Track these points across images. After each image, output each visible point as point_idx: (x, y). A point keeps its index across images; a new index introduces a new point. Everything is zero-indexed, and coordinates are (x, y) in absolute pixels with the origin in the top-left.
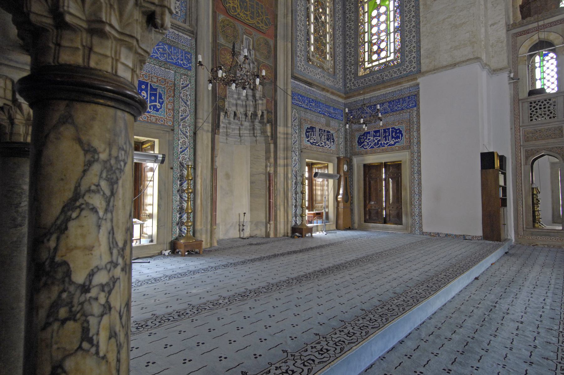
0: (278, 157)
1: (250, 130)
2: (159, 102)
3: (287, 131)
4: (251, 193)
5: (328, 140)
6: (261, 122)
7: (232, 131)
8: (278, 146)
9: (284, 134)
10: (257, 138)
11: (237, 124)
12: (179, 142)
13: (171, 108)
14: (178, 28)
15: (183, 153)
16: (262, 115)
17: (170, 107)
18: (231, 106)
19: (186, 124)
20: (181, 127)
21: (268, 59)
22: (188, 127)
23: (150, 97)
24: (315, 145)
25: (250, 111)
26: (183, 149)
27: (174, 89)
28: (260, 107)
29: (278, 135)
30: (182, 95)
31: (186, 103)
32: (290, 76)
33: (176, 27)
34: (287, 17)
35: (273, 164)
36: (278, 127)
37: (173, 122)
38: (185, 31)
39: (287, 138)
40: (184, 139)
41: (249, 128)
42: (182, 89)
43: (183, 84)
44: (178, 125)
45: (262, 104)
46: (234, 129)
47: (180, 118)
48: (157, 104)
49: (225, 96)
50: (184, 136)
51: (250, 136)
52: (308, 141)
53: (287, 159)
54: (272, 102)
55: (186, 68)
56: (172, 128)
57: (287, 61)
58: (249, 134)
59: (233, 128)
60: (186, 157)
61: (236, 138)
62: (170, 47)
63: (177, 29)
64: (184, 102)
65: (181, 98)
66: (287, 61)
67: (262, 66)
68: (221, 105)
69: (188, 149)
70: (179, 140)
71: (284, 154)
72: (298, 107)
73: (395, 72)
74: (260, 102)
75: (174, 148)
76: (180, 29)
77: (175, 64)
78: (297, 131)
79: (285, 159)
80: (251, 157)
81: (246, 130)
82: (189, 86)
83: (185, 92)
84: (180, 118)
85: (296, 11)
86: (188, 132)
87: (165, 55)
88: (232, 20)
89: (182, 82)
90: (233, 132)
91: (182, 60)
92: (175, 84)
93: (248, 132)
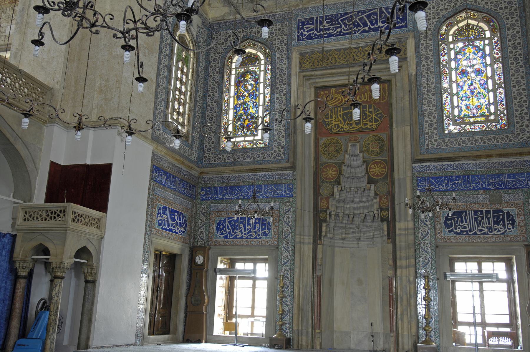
2: (268, 229)
5: (497, 223)
7: (364, 234)
13: (276, 231)
17: (275, 230)
20: (284, 244)
21: (379, 154)
23: (262, 226)
24: (467, 234)
29: (398, 232)
30: (285, 219)
31: (288, 225)
36: (397, 223)
37: (278, 242)
40: (286, 254)
42: (285, 214)
43: (286, 210)
48: (267, 230)
52: (452, 231)
54: (387, 198)
55: (289, 197)
56: (277, 246)
59: (364, 231)
60: (287, 268)
62: (276, 185)
64: (287, 224)
67: (371, 165)
69: (289, 261)
70: (282, 255)
73: (452, 143)
75: (278, 261)
77: (280, 196)
81: (377, 231)
82: (291, 210)
86: (290, 247)
87: (273, 193)
89: (285, 209)
90: (365, 235)
91: (285, 192)
92: (279, 212)
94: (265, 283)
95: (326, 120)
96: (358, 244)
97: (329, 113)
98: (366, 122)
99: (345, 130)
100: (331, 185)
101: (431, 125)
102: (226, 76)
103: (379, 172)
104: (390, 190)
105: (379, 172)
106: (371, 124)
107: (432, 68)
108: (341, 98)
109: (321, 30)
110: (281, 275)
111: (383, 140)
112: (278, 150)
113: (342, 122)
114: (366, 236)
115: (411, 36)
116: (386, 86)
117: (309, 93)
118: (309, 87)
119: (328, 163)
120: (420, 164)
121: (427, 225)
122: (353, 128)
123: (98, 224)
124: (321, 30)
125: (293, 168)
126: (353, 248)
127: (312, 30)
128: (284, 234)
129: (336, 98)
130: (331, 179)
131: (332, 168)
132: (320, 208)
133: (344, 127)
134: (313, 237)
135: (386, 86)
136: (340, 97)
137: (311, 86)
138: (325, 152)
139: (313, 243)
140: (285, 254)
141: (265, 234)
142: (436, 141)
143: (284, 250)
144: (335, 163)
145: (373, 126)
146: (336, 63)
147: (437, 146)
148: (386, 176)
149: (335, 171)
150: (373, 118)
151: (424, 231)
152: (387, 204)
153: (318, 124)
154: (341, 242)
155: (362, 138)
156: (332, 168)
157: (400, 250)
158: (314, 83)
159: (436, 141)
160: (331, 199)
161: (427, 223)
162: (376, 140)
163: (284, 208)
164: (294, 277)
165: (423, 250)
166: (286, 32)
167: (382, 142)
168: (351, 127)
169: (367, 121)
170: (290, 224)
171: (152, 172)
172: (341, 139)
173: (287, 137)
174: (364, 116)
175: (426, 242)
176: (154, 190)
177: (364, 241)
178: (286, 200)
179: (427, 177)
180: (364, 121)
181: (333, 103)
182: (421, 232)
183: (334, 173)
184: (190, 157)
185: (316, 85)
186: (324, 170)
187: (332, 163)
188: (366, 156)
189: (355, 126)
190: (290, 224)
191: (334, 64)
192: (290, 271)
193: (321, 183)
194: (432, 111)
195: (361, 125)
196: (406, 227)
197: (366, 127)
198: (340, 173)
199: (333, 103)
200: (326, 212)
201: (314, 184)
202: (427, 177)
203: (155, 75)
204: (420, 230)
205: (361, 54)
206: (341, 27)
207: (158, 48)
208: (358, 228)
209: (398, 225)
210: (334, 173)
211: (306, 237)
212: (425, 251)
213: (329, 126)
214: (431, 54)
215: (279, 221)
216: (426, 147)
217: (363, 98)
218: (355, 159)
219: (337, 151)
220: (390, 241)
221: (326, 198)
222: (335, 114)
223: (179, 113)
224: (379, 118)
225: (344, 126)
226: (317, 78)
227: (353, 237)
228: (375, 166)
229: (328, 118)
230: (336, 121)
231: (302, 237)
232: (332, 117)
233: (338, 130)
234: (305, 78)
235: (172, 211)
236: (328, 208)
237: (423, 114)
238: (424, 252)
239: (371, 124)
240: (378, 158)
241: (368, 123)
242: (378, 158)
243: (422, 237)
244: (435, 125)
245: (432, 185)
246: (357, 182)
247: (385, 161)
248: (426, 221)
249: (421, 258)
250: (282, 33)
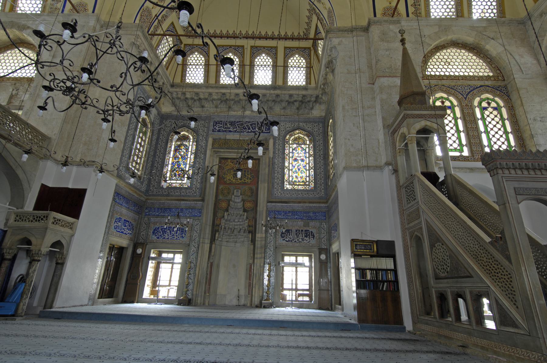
29: (257, 239)
46: (239, 238)
54: (253, 220)
62: (192, 209)
94: (179, 266)
102: (169, 146)
109: (225, 128)
123: (71, 226)
124: (225, 128)
125: (203, 200)
127: (221, 127)
141: (183, 237)
142: (280, 192)
151: (270, 239)
159: (280, 192)
160: (222, 219)
166: (206, 126)
171: (114, 196)
176: (114, 207)
178: (197, 218)
184: (141, 189)
190: (198, 232)
198: (229, 205)
200: (219, 226)
203: (124, 139)
206: (236, 128)
207: (128, 123)
208: (236, 236)
223: (137, 163)
235: (125, 220)
236: (220, 224)
250: (204, 126)
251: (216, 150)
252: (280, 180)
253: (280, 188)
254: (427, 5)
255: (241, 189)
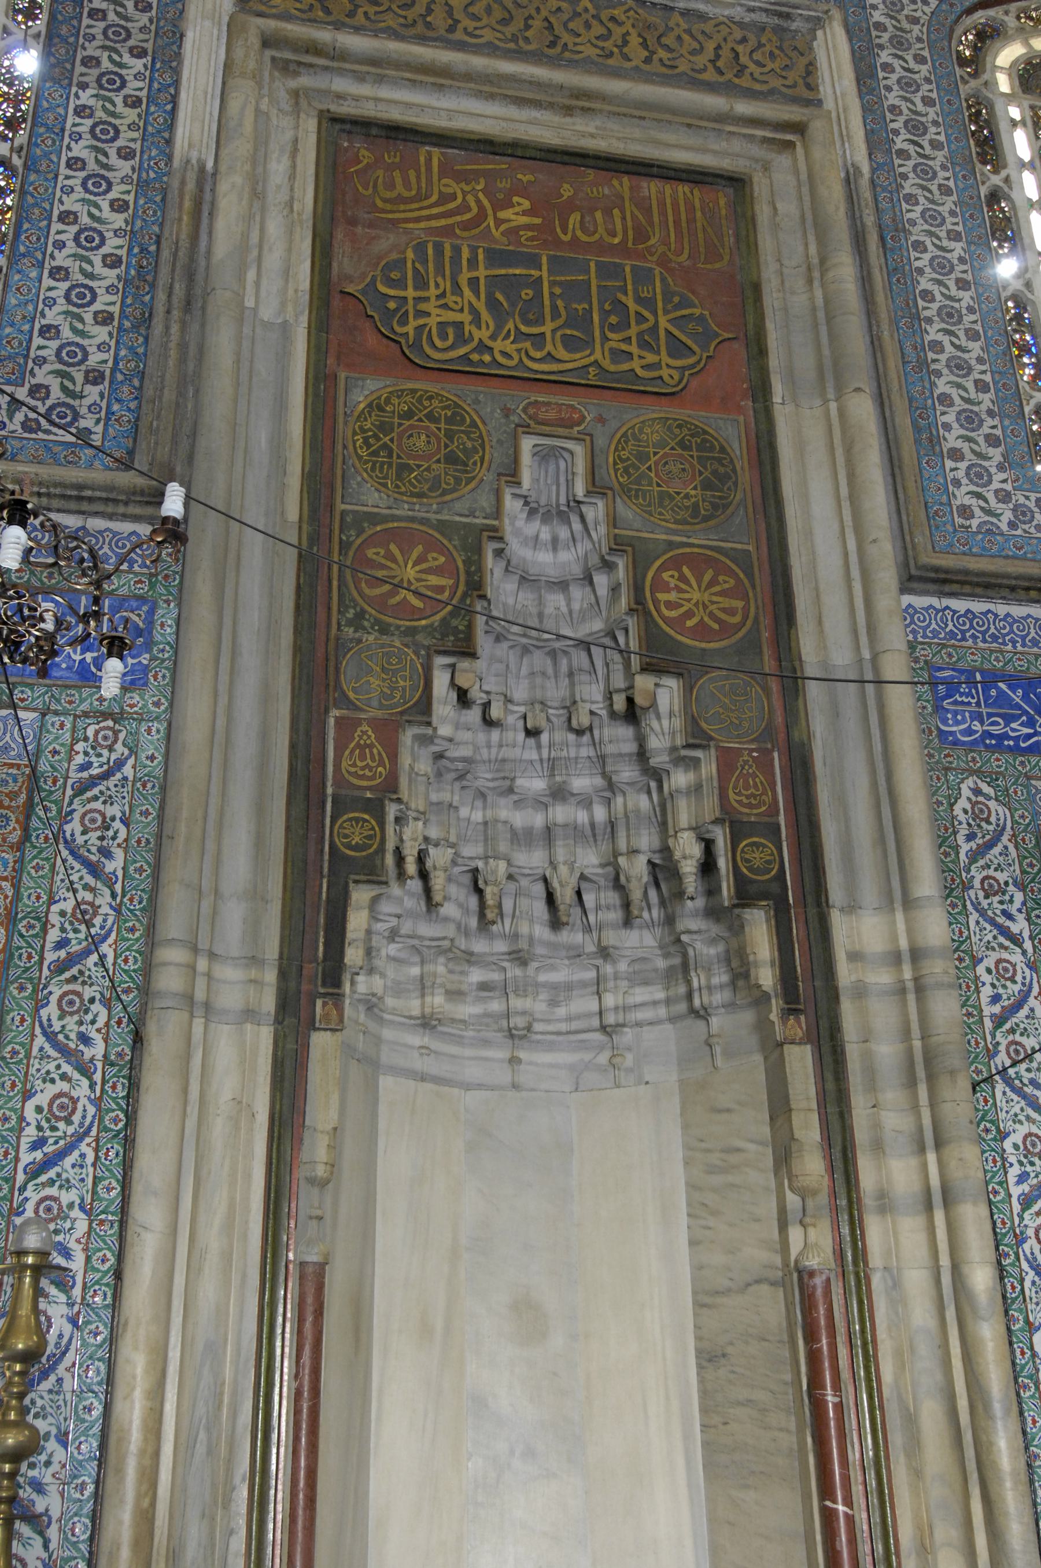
0: (861, 1135)
1: (669, 976)
3: (910, 931)
4: (705, 1444)
6: (714, 912)
7: (553, 1003)
8: (853, 1052)
9: (895, 958)
10: (714, 1021)
11: (576, 954)
12: (30, 1106)
14: (80, 498)
15: (52, 1173)
16: (708, 867)
18: (503, 847)
19: (88, 992)
20: (51, 1011)
21: (706, 519)
22: (96, 1007)
25: (634, 852)
26: (49, 1149)
27: (30, 805)
28: (684, 814)
29: (845, 974)
30: (74, 827)
31: (95, 870)
32: (887, 576)
33: (63, 497)
34: (824, 270)
35: (823, 1198)
38: (115, 501)
39: (920, 989)
40: (62, 1086)
41: (661, 964)
42: (79, 791)
43: (85, 767)
44: (28, 1005)
45: (697, 789)
46: (559, 993)
47: (50, 957)
49: (390, 786)
50: (67, 1068)
51: (672, 1019)
53: (939, 1144)
54: (766, 767)
57: (854, 499)
58: (668, 1002)
59: (554, 987)
61: (583, 1046)
63: (73, 505)
65: (977, 906)
66: (854, 499)
67: (662, 568)
68: (356, 840)
69: (86, 1148)
71: (915, 1108)
72: (998, 762)
74: (680, 779)
76: (90, 499)
78: (1020, 926)
79: (922, 1150)
80: (687, 1163)
81: (646, 983)
82: (128, 770)
83: (97, 805)
84: (50, 957)
85: (901, 229)
86: (98, 1039)
88: (432, 388)
89: (79, 759)
90: (561, 1011)
93: (661, 995)
95: (383, 289)
96: (514, 1061)
97: (404, 261)
98: (624, 347)
99: (500, 359)
100: (417, 647)
101: (970, 420)
103: (711, 615)
104: (779, 719)
105: (711, 615)
106: (651, 358)
107: (942, 174)
108: (478, 201)
110: (21, 1253)
111: (723, 449)
112: (64, 389)
113: (485, 316)
114: (569, 1019)
115: (836, 14)
116: (722, 202)
117: (289, 135)
118: (287, 108)
119: (394, 518)
120: (935, 601)
121: (1016, 940)
122: (550, 357)
126: (480, 1086)
128: (53, 935)
129: (445, 198)
130: (415, 614)
131: (419, 549)
132: (339, 781)
133: (498, 345)
134: (283, 975)
135: (722, 202)
136: (470, 199)
137: (303, 103)
138: (375, 453)
139: (278, 1021)
140: (52, 1090)
142: (1004, 497)
143: (43, 1057)
144: (442, 526)
145: (665, 373)
146: (451, 29)
147: (1012, 525)
148: (751, 645)
149: (438, 571)
150: (662, 334)
151: (1003, 972)
152: (767, 799)
153: (336, 302)
154: (416, 1039)
155: (601, 420)
156: (419, 549)
157: (872, 1085)
158: (326, 93)
159: (1004, 497)
161: (1015, 928)
162: (683, 445)
163: (71, 752)
164: (118, 1274)
165: (1014, 1089)
167: (719, 460)
168: (538, 355)
169: (628, 340)
170: (114, 865)
172: (477, 401)
173: (135, 327)
174: (608, 313)
175: (1023, 1040)
177: (551, 1047)
179: (982, 672)
180: (610, 335)
181: (429, 218)
182: (986, 978)
183: (434, 580)
185: (333, 108)
186: (370, 553)
187: (424, 521)
188: (630, 515)
189: (562, 353)
190: (114, 865)
191: (442, 32)
192: (82, 1226)
193: (349, 631)
194: (966, 356)
195: (598, 355)
196: (904, 944)
197: (625, 367)
198: (476, 586)
199: (429, 218)
201: (297, 631)
202: (982, 672)
204: (980, 970)
205: (588, 26)
208: (520, 958)
209: (840, 925)
210: (434, 580)
211: (228, 973)
212: (1024, 1096)
213: (404, 321)
214: (932, 116)
215: (26, 837)
216: (959, 520)
217: (601, 230)
218: (545, 535)
219: (451, 459)
220: (797, 1027)
221: (377, 725)
222: (440, 270)
224: (693, 335)
225: (493, 337)
226: (341, 72)
227: (487, 1015)
228: (683, 578)
229: (401, 284)
230: (445, 306)
231: (202, 964)
232: (421, 283)
233: (462, 351)
234: (269, 53)
237: (923, 364)
238: (1018, 1105)
239: (651, 358)
240: (700, 539)
241: (634, 349)
242: (700, 539)
243: (997, 1009)
244: (990, 422)
245: (1014, 718)
246: (544, 674)
247: (742, 559)
248: (1010, 917)
249: (1008, 1144)
251: (295, 30)
252: (981, 386)
253: (996, 454)
254: (1039, 36)
255: (586, 437)
